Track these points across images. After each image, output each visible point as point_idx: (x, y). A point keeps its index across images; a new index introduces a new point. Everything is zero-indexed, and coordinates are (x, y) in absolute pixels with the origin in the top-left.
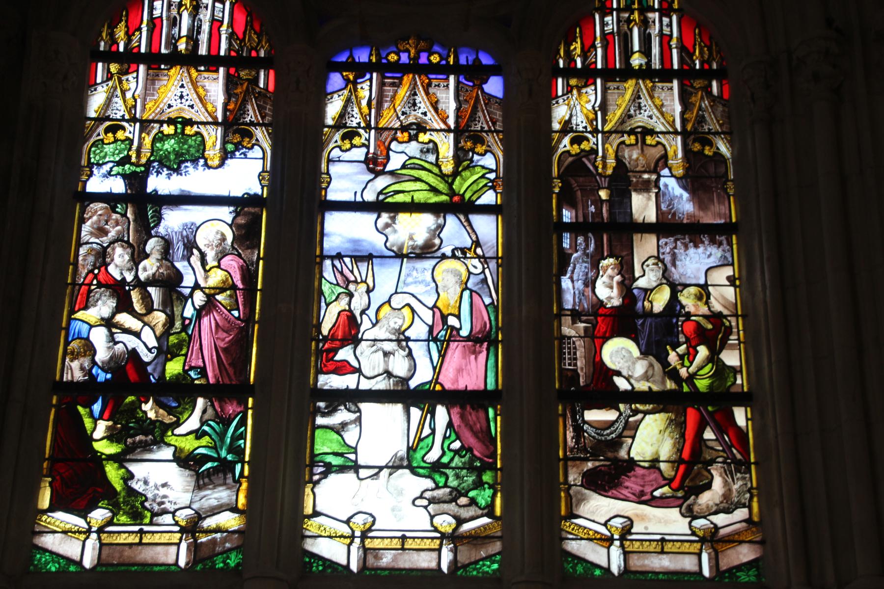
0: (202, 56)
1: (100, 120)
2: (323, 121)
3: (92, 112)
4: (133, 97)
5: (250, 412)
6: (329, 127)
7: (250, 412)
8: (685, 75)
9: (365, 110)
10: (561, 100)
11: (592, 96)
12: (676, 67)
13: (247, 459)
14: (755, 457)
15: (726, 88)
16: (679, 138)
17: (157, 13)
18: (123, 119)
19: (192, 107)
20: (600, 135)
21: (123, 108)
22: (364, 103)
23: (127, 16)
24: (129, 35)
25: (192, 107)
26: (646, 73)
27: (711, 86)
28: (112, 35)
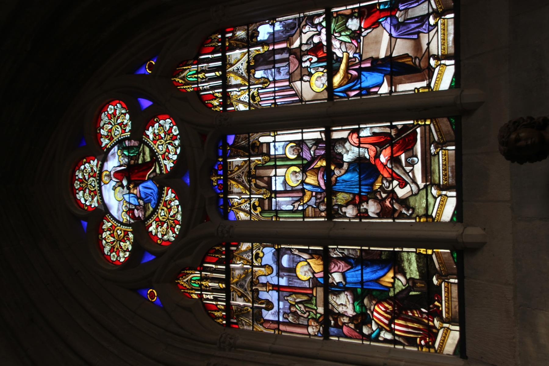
0: (226, 277)
1: (249, 104)
2: (248, 220)
3: (247, 218)
4: (239, 91)
5: (339, 247)
6: (251, 218)
7: (339, 247)
8: (224, 50)
9: (243, 200)
10: (237, 107)
11: (234, 92)
12: (224, 267)
13: (357, 127)
14: (364, 25)
15: (228, 30)
16: (250, 49)
17: (211, 297)
18: (250, 204)
19: (242, 64)
20: (252, 196)
21: (245, 204)
22: (239, 93)
23: (211, 311)
24: (219, 310)
25: (242, 64)
26: (223, 68)
27: (228, 37)
28: (219, 318)
